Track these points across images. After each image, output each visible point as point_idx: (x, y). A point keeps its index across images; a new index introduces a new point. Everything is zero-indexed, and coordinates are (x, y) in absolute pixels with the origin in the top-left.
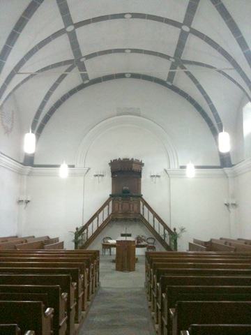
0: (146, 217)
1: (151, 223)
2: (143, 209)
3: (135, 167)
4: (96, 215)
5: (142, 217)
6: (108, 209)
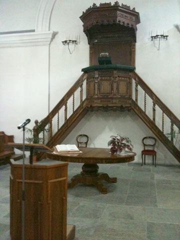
0: (141, 104)
1: (149, 113)
2: (137, 90)
3: (121, 19)
4: (63, 102)
5: (135, 104)
6: (81, 91)
